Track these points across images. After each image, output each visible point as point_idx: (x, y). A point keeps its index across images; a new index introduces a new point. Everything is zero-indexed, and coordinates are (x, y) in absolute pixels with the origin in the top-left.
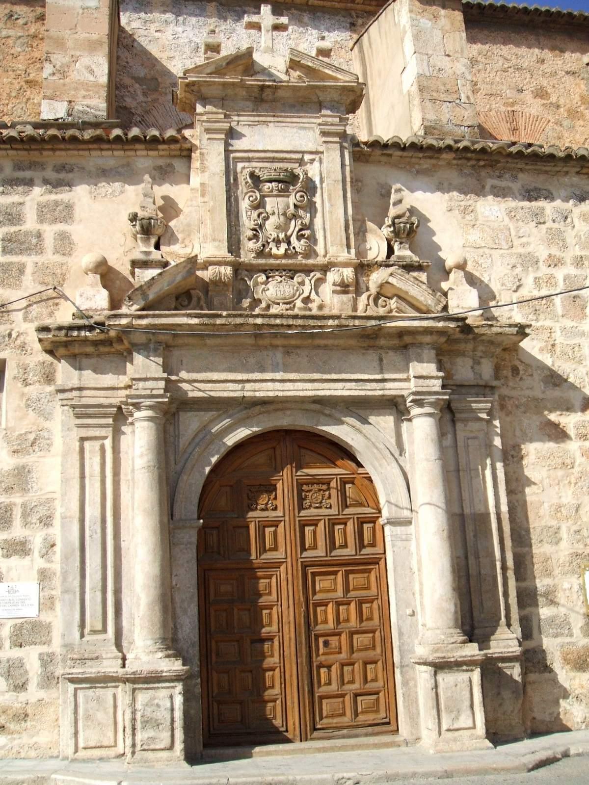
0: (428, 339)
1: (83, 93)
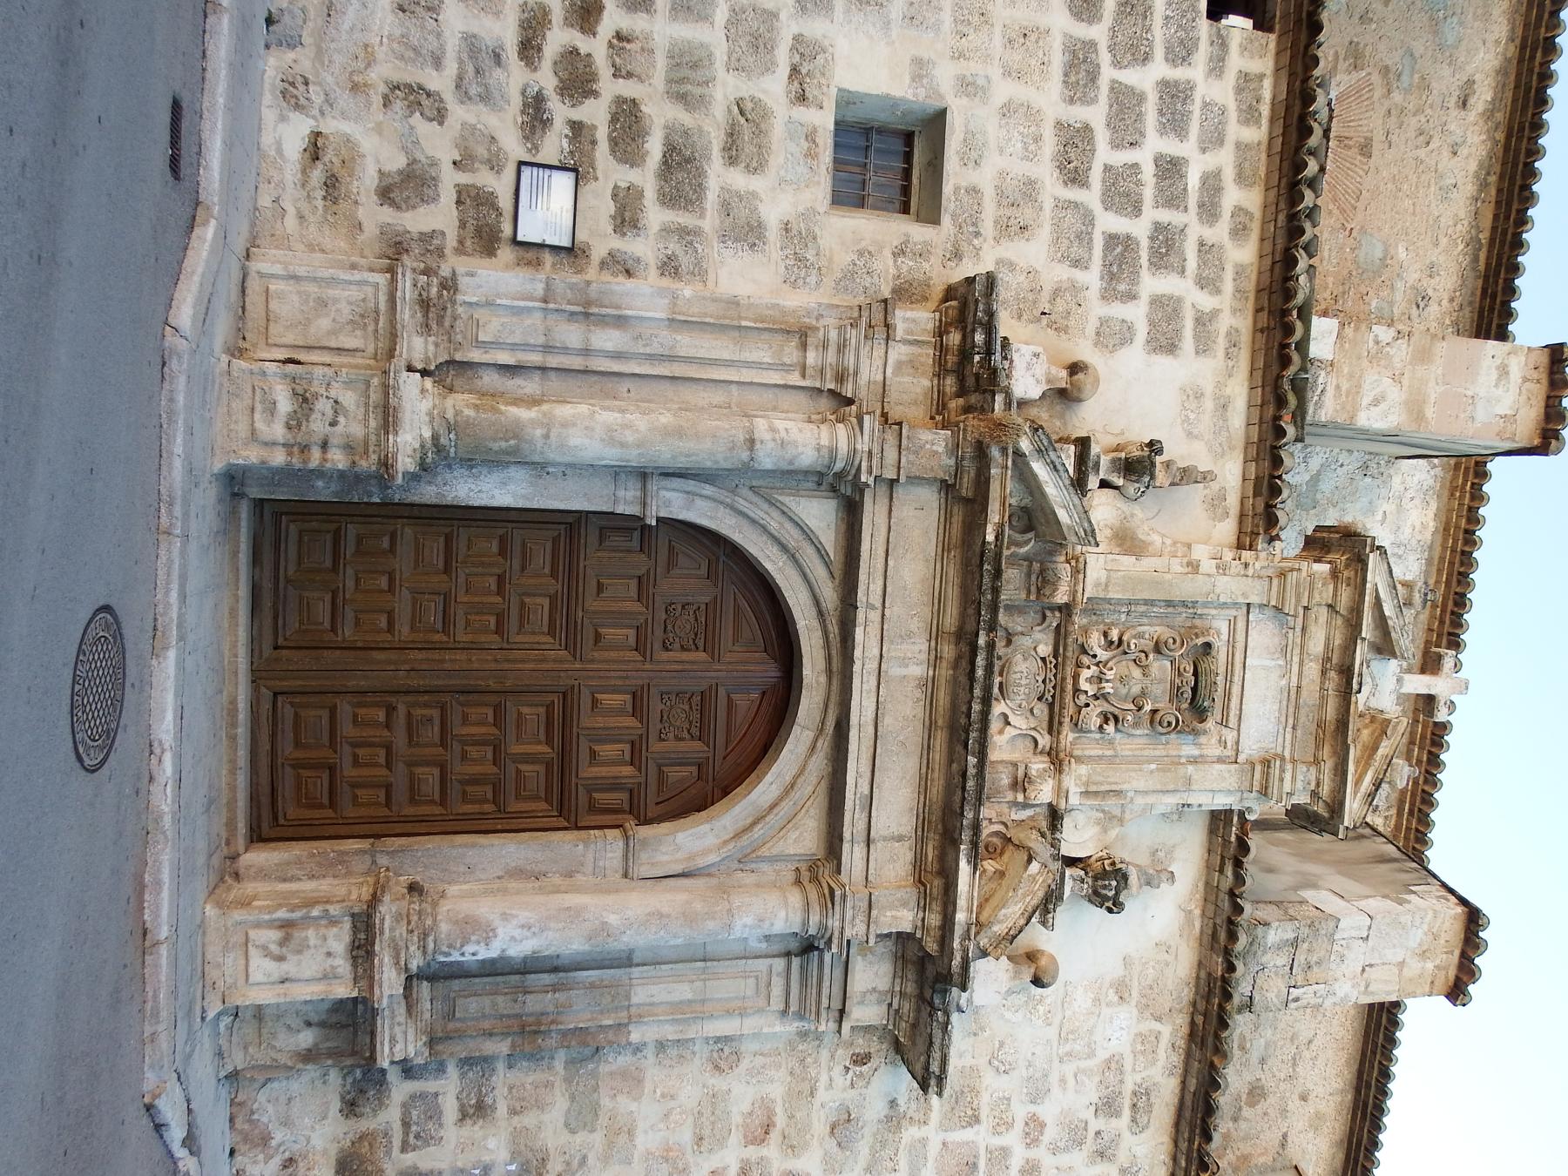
0: (934, 920)
1: (1345, 386)
